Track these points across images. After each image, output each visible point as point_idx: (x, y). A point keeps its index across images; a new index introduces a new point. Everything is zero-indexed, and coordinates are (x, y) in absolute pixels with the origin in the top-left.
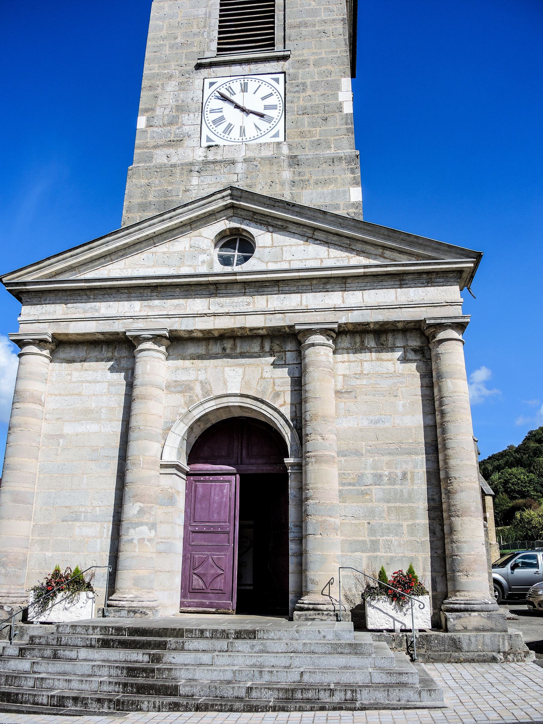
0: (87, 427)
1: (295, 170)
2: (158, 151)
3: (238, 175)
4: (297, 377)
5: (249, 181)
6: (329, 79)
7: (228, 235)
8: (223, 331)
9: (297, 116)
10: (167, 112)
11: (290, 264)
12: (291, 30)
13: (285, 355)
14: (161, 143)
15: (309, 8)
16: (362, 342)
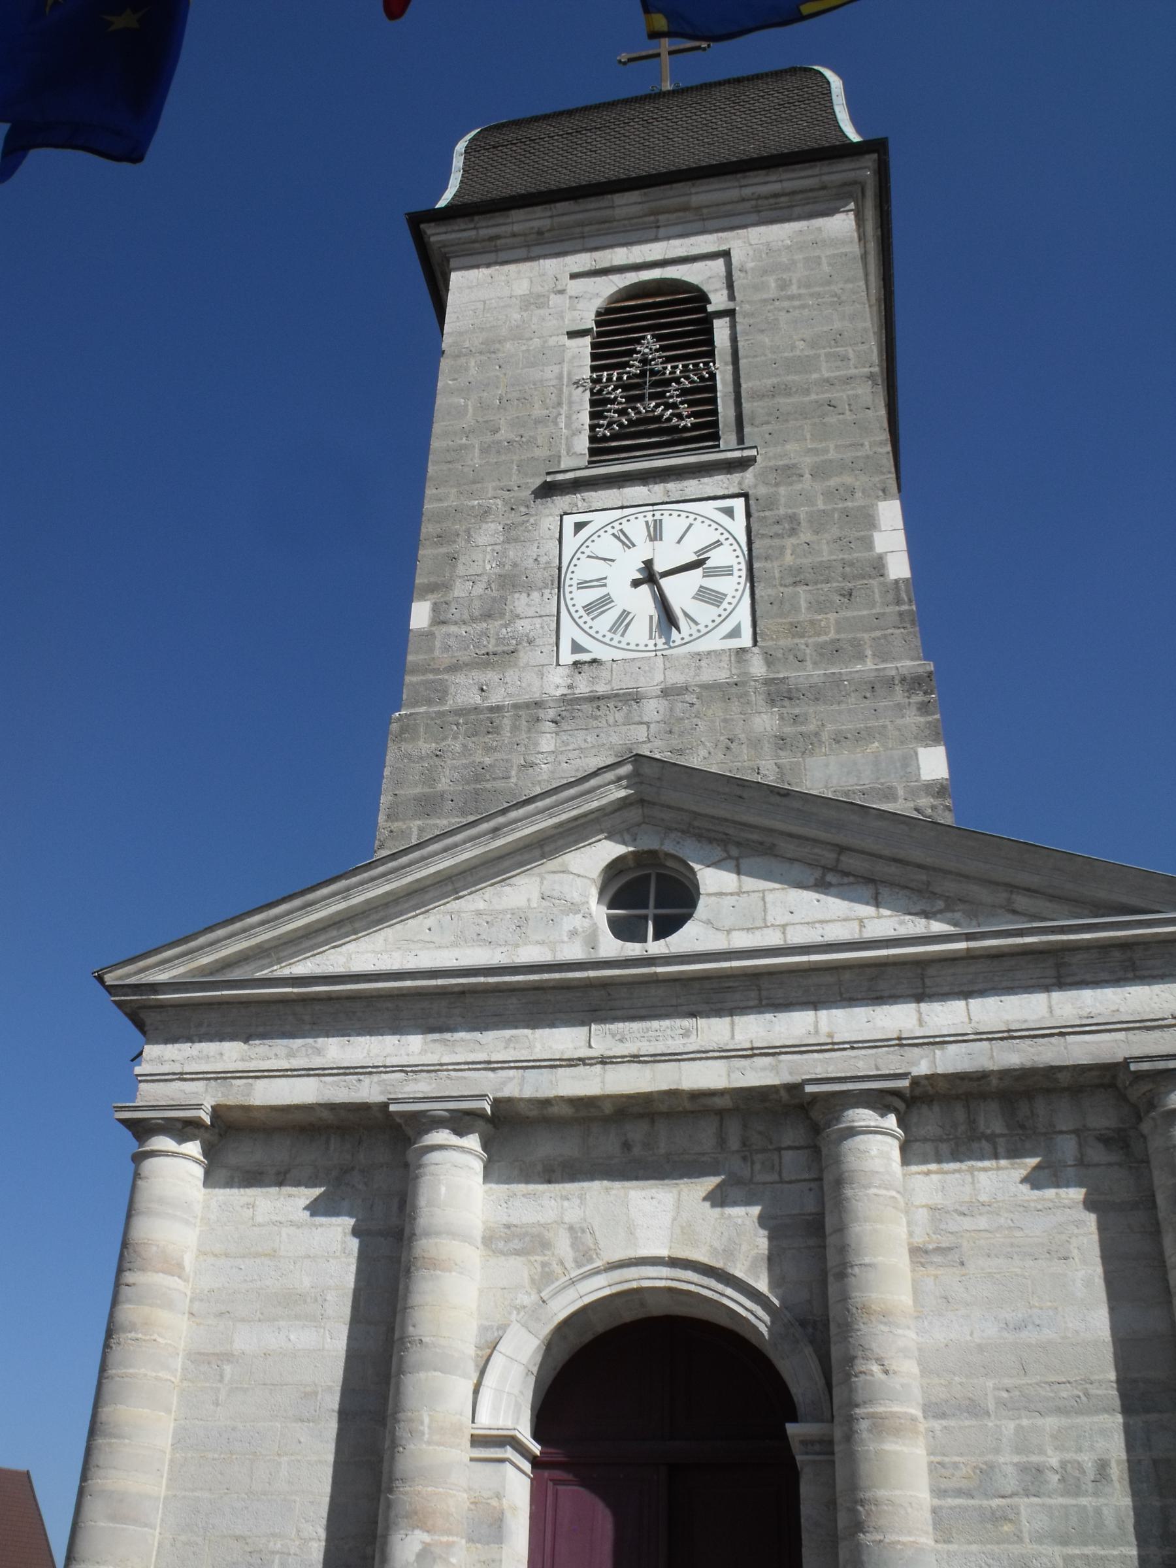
0: (292, 1337)
1: (784, 710)
2: (460, 678)
3: (648, 727)
4: (813, 1214)
5: (675, 742)
6: (849, 504)
7: (630, 868)
8: (624, 1100)
9: (782, 589)
10: (479, 590)
11: (784, 933)
12: (755, 404)
13: (780, 1158)
14: (466, 659)
15: (791, 354)
16: (972, 1122)
